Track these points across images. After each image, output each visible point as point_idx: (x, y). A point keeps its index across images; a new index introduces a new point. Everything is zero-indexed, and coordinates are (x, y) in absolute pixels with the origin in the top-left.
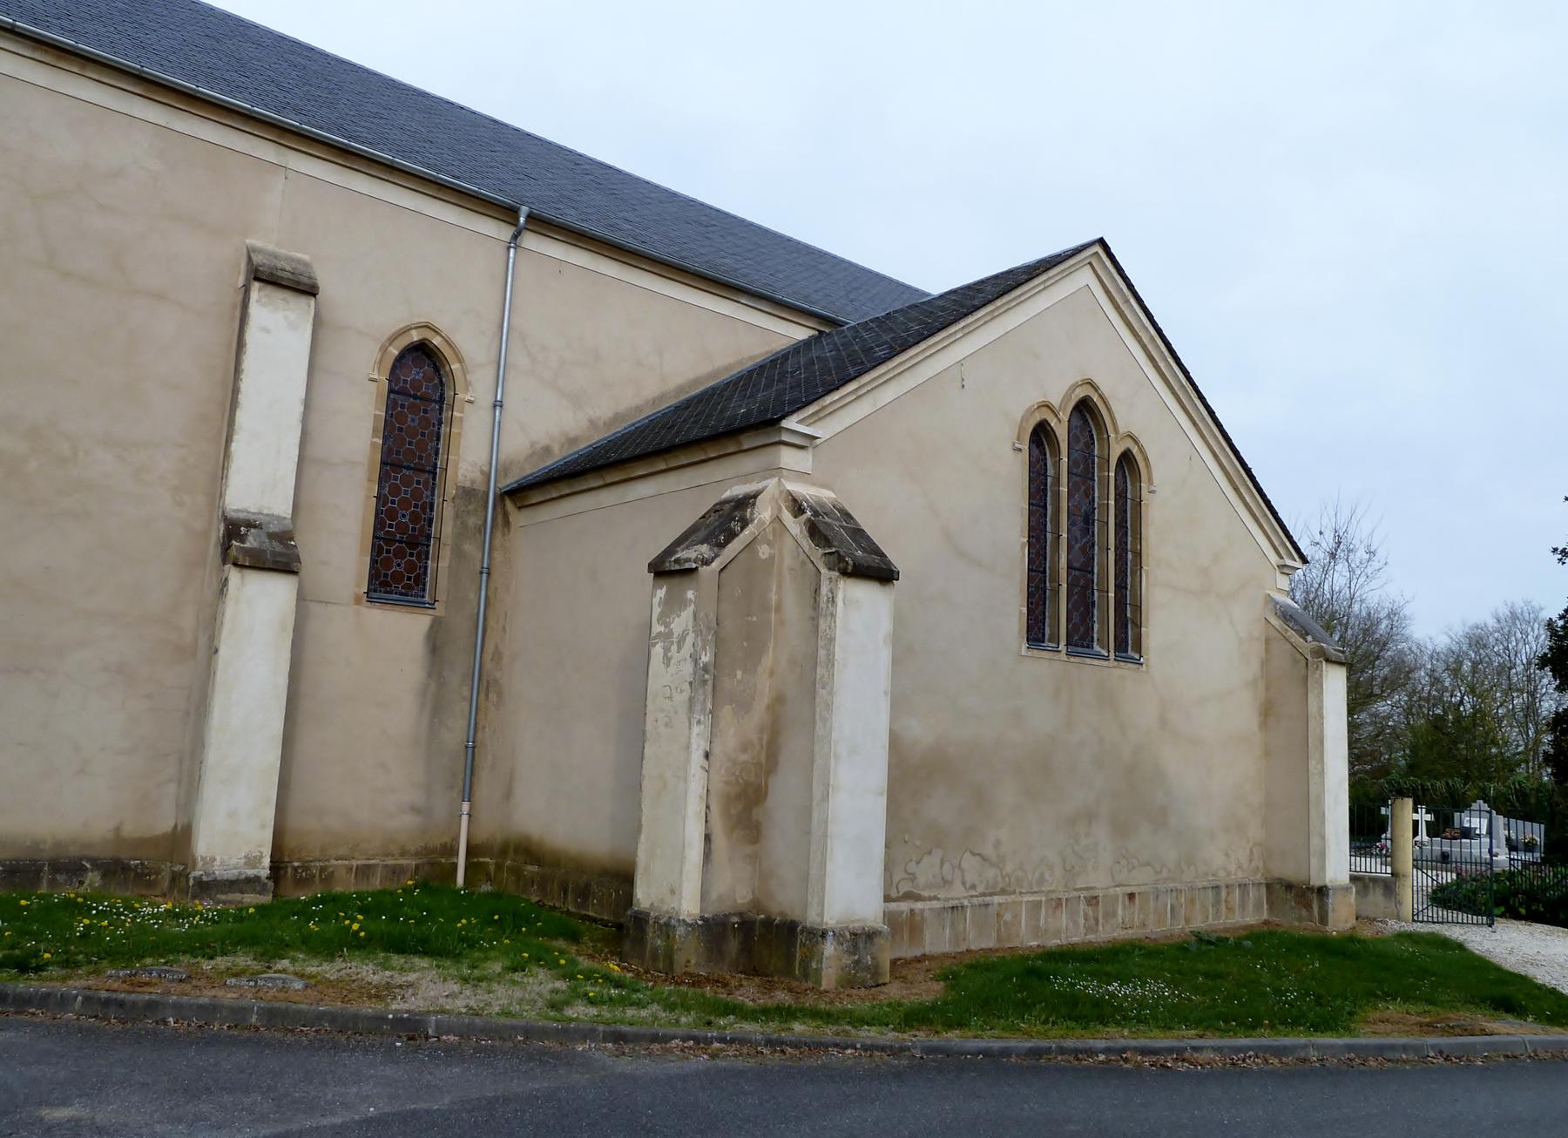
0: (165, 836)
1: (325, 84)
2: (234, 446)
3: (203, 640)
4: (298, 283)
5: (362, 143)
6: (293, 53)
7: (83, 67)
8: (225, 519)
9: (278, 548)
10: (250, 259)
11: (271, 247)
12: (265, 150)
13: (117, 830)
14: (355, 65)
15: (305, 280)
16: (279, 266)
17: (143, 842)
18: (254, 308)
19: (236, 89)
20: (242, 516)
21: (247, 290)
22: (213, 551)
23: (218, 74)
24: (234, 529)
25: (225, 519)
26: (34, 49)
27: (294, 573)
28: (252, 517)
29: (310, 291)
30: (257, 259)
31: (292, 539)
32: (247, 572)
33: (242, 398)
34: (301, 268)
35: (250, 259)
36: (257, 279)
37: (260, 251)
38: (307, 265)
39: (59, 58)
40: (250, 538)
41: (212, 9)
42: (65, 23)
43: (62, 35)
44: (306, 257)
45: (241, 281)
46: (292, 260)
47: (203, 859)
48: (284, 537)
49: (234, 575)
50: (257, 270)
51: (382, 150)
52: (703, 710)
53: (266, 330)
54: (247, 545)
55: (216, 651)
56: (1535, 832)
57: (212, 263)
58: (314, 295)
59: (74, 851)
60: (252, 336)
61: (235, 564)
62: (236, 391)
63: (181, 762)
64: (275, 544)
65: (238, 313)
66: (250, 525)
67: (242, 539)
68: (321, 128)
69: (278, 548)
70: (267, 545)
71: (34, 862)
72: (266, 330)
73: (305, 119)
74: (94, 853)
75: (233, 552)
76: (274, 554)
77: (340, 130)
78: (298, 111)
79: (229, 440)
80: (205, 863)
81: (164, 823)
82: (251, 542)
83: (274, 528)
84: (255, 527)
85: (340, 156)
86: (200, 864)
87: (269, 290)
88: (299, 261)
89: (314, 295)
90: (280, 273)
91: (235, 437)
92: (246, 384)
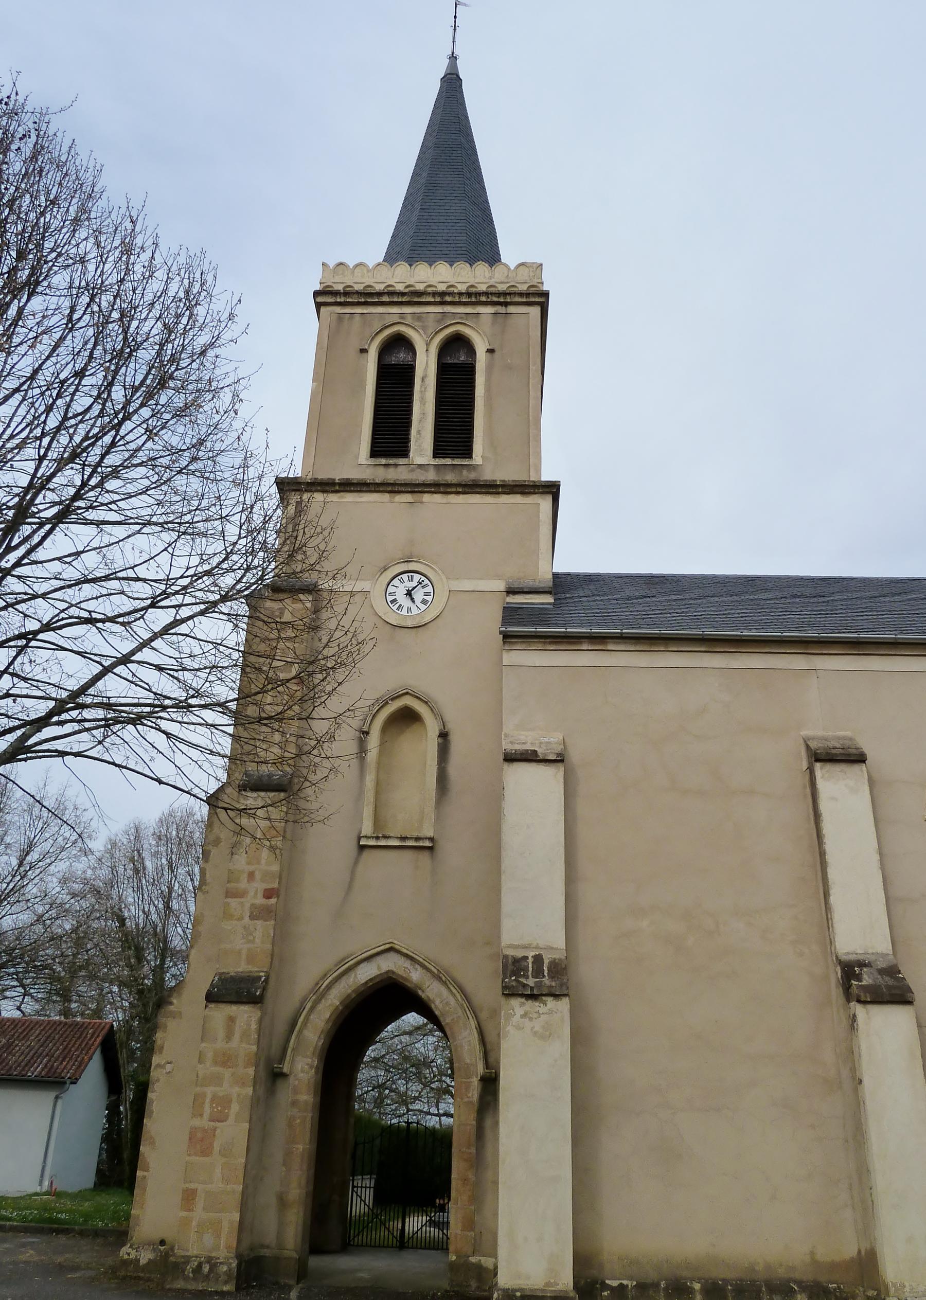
0: (852, 1259)
1: (821, 599)
2: (832, 899)
3: (845, 1073)
4: (849, 755)
5: (867, 633)
6: (789, 586)
7: (666, 645)
8: (840, 962)
9: (891, 982)
10: (808, 747)
11: (820, 733)
12: (798, 662)
13: (812, 1253)
14: (835, 578)
15: (854, 751)
16: (831, 746)
17: (834, 1266)
18: (821, 784)
19: (765, 625)
20: (852, 957)
21: (811, 770)
22: (836, 992)
23: (748, 619)
24: (850, 971)
25: (840, 962)
26: (636, 644)
27: (909, 1003)
28: (861, 957)
29: (860, 759)
30: (813, 745)
31: (899, 972)
32: (869, 1007)
33: (829, 858)
34: (848, 743)
35: (808, 747)
36: (817, 760)
37: (813, 738)
38: (851, 739)
39: (651, 644)
40: (865, 976)
41: (727, 577)
42: (648, 621)
43: (762, 630)
44: (848, 733)
45: (805, 765)
46: (839, 738)
47: (894, 1285)
48: (892, 971)
49: (860, 1011)
50: (816, 754)
51: (884, 633)
52: (7, 1064)
53: (834, 799)
54: (864, 983)
55: (860, 1082)
56: (408, 1209)
57: (783, 758)
58: (864, 761)
59: (782, 1272)
60: (823, 806)
61: (859, 1001)
62: (822, 854)
63: (851, 1187)
64: (887, 978)
65: (808, 791)
66: (862, 964)
67: (859, 978)
68: (833, 632)
69: (891, 982)
70: (880, 980)
71: (753, 1282)
72: (834, 799)
73: (819, 629)
74: (797, 1276)
75: (854, 990)
76: (888, 987)
77: (847, 629)
78: (812, 625)
79: (826, 895)
80: (897, 1290)
81: (849, 1249)
82: (867, 980)
83: (881, 964)
84: (865, 965)
85: (854, 648)
86: (892, 1290)
87: (829, 767)
88: (844, 738)
89: (864, 761)
90: (834, 751)
91: (831, 892)
92: (829, 847)
